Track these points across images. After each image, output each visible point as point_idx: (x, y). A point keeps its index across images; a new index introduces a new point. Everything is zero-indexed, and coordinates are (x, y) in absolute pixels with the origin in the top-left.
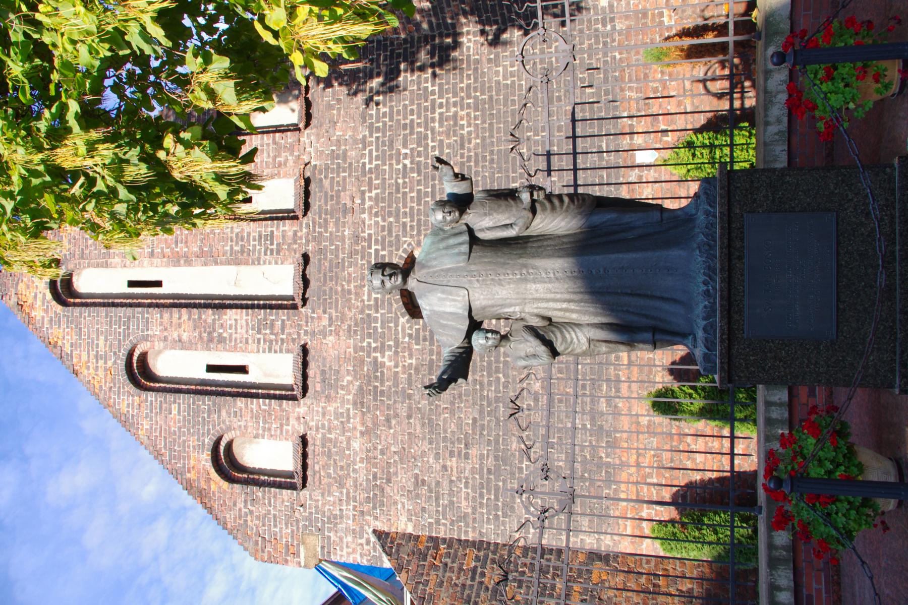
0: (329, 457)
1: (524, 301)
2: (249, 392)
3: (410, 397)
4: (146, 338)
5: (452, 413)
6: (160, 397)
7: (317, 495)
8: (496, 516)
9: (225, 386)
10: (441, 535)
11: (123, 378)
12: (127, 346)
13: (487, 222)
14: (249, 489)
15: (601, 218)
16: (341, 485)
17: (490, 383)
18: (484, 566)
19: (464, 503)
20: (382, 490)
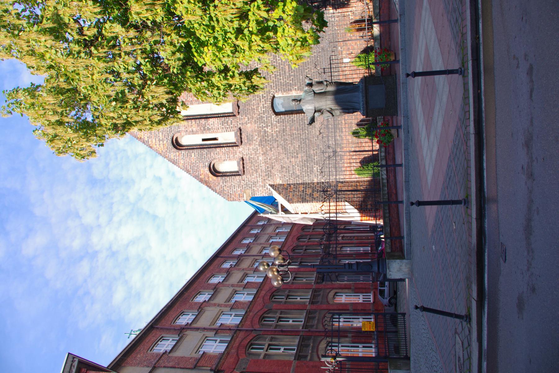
0: (252, 163)
1: (326, 105)
2: (220, 146)
3: (277, 141)
4: (179, 132)
5: (292, 144)
6: (187, 152)
7: (249, 176)
8: (308, 175)
9: (210, 145)
10: (291, 183)
11: (171, 146)
12: (171, 135)
13: (317, 89)
14: (224, 178)
15: (340, 87)
16: (257, 172)
17: (303, 134)
18: (306, 188)
19: (297, 172)
20: (271, 171)
